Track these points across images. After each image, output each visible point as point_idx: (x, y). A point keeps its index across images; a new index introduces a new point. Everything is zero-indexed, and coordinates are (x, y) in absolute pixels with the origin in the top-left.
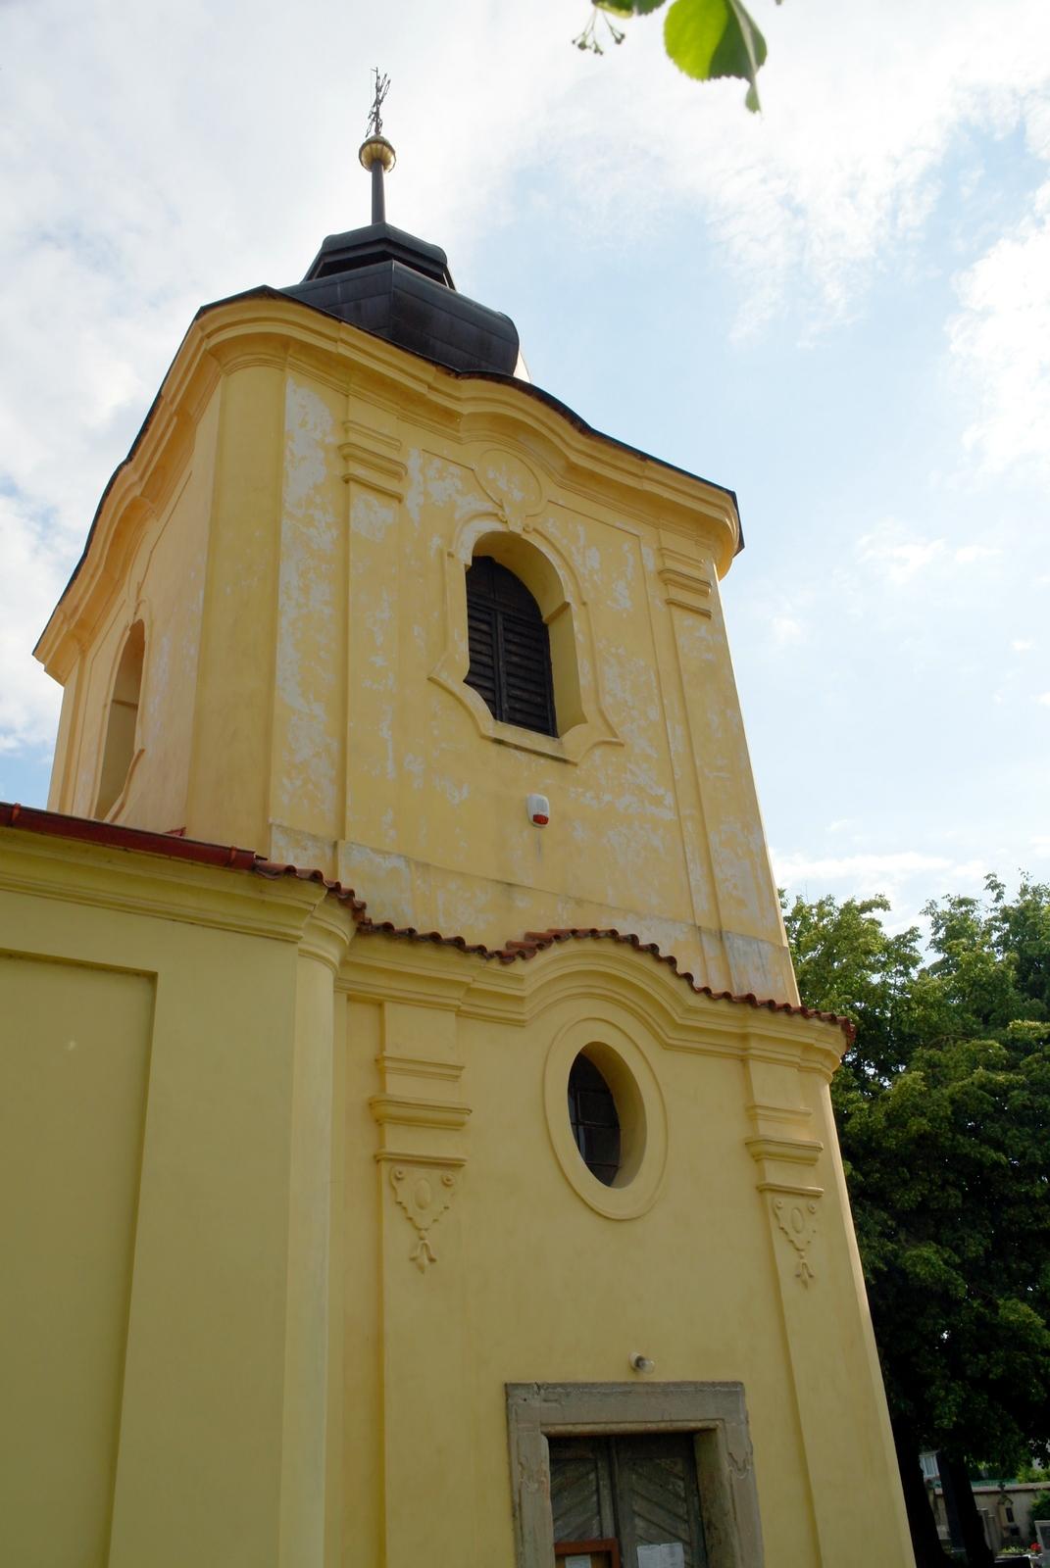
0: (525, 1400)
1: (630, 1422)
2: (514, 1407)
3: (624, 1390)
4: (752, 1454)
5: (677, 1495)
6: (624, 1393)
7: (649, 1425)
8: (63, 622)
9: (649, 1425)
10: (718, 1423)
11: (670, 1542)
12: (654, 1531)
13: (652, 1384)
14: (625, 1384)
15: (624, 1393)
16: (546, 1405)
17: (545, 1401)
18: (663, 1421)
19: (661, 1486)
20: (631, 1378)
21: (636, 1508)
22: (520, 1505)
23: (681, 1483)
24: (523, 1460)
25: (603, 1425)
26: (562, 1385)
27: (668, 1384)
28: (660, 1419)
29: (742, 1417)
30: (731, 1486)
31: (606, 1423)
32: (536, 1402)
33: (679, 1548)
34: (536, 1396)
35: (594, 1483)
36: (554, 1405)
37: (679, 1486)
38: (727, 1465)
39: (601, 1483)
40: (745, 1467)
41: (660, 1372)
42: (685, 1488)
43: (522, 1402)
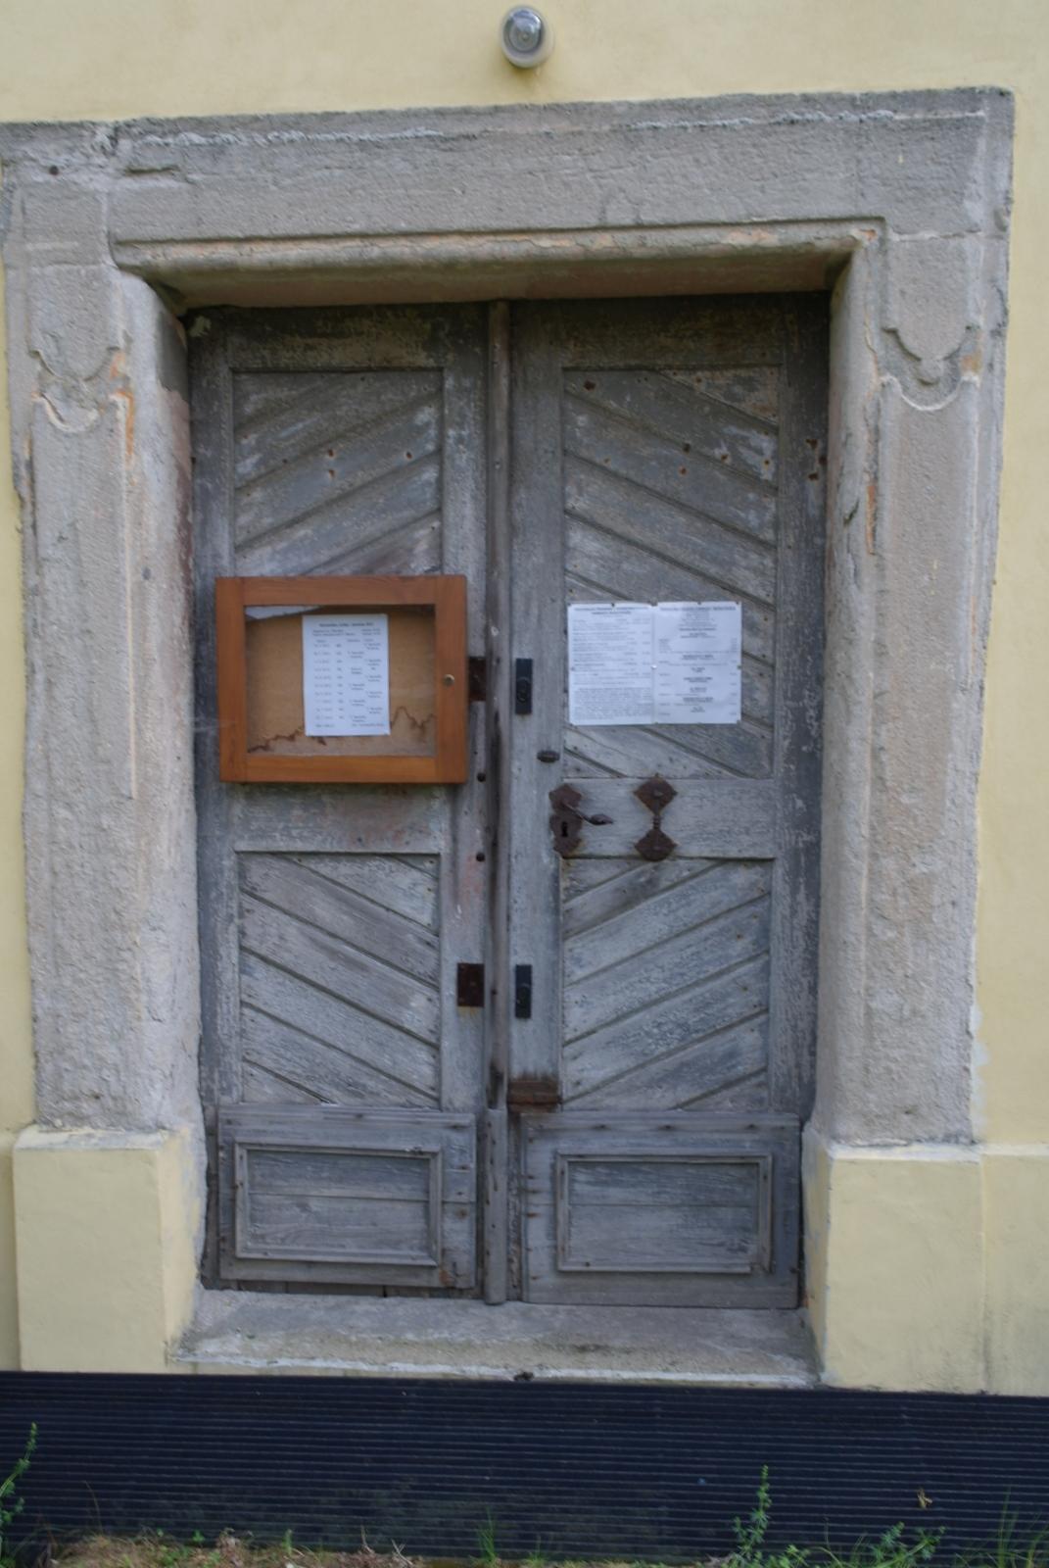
0: (54, 171)
1: (551, 231)
2: (18, 193)
3: (450, 133)
4: (999, 332)
5: (752, 479)
6: (446, 142)
7: (545, 242)
8: (293, 1196)
9: (545, 242)
10: (854, 231)
11: (699, 599)
12: (636, 567)
13: (577, 110)
14: (465, 112)
15: (446, 142)
16: (131, 184)
17: (134, 172)
18: (603, 228)
19: (687, 448)
20: (508, 95)
21: (578, 503)
22: (30, 465)
23: (766, 443)
24: (43, 345)
25: (357, 243)
26: (199, 124)
27: (650, 108)
28: (594, 222)
29: (977, 211)
30: (876, 434)
31: (363, 236)
32: (100, 181)
33: (726, 619)
34: (100, 160)
35: (433, 432)
36: (165, 182)
37: (759, 452)
38: (870, 367)
39: (451, 432)
40: (954, 380)
41: (584, 70)
42: (776, 455)
43: (42, 177)
